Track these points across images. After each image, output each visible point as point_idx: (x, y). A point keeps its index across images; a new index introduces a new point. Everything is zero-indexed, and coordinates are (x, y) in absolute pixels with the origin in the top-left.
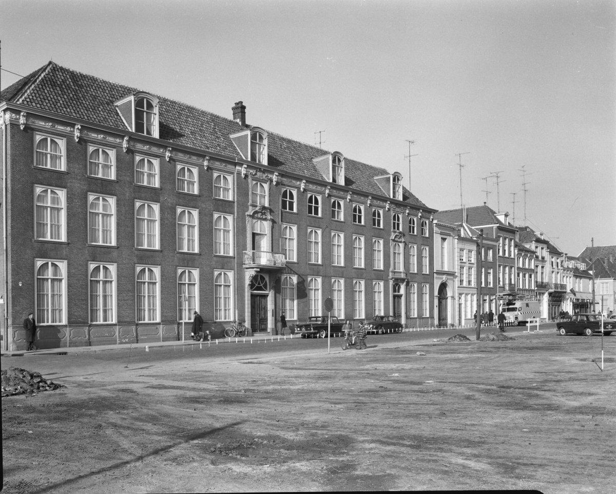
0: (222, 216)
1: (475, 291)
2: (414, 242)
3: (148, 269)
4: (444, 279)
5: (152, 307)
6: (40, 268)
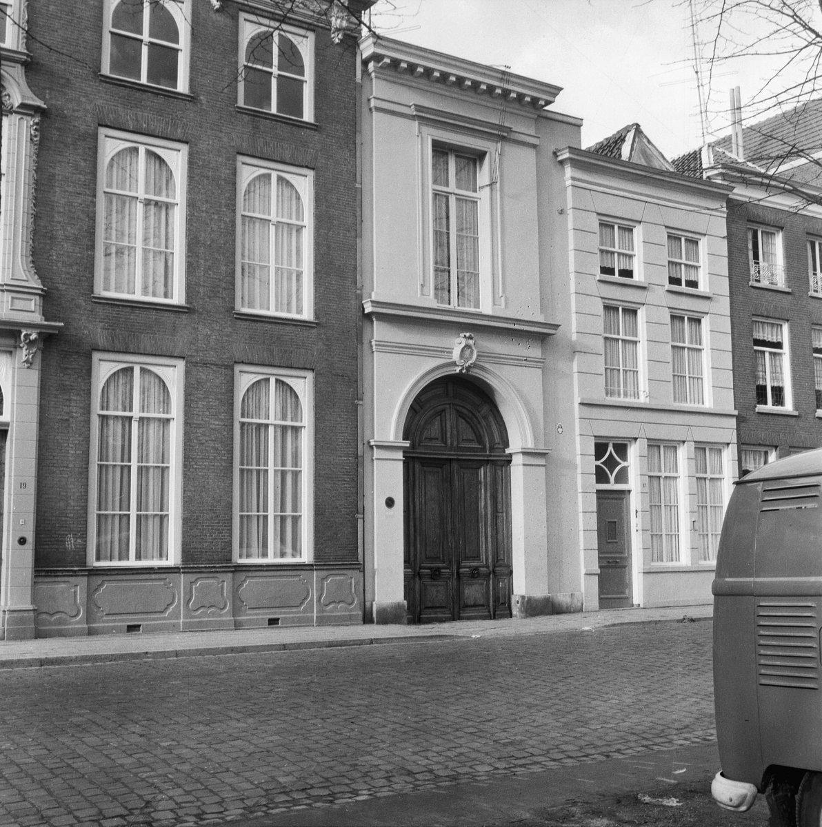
0: (274, 175)
1: (727, 431)
2: (158, 127)
3: (277, 381)
4: (456, 355)
5: (289, 512)
6: (108, 382)
